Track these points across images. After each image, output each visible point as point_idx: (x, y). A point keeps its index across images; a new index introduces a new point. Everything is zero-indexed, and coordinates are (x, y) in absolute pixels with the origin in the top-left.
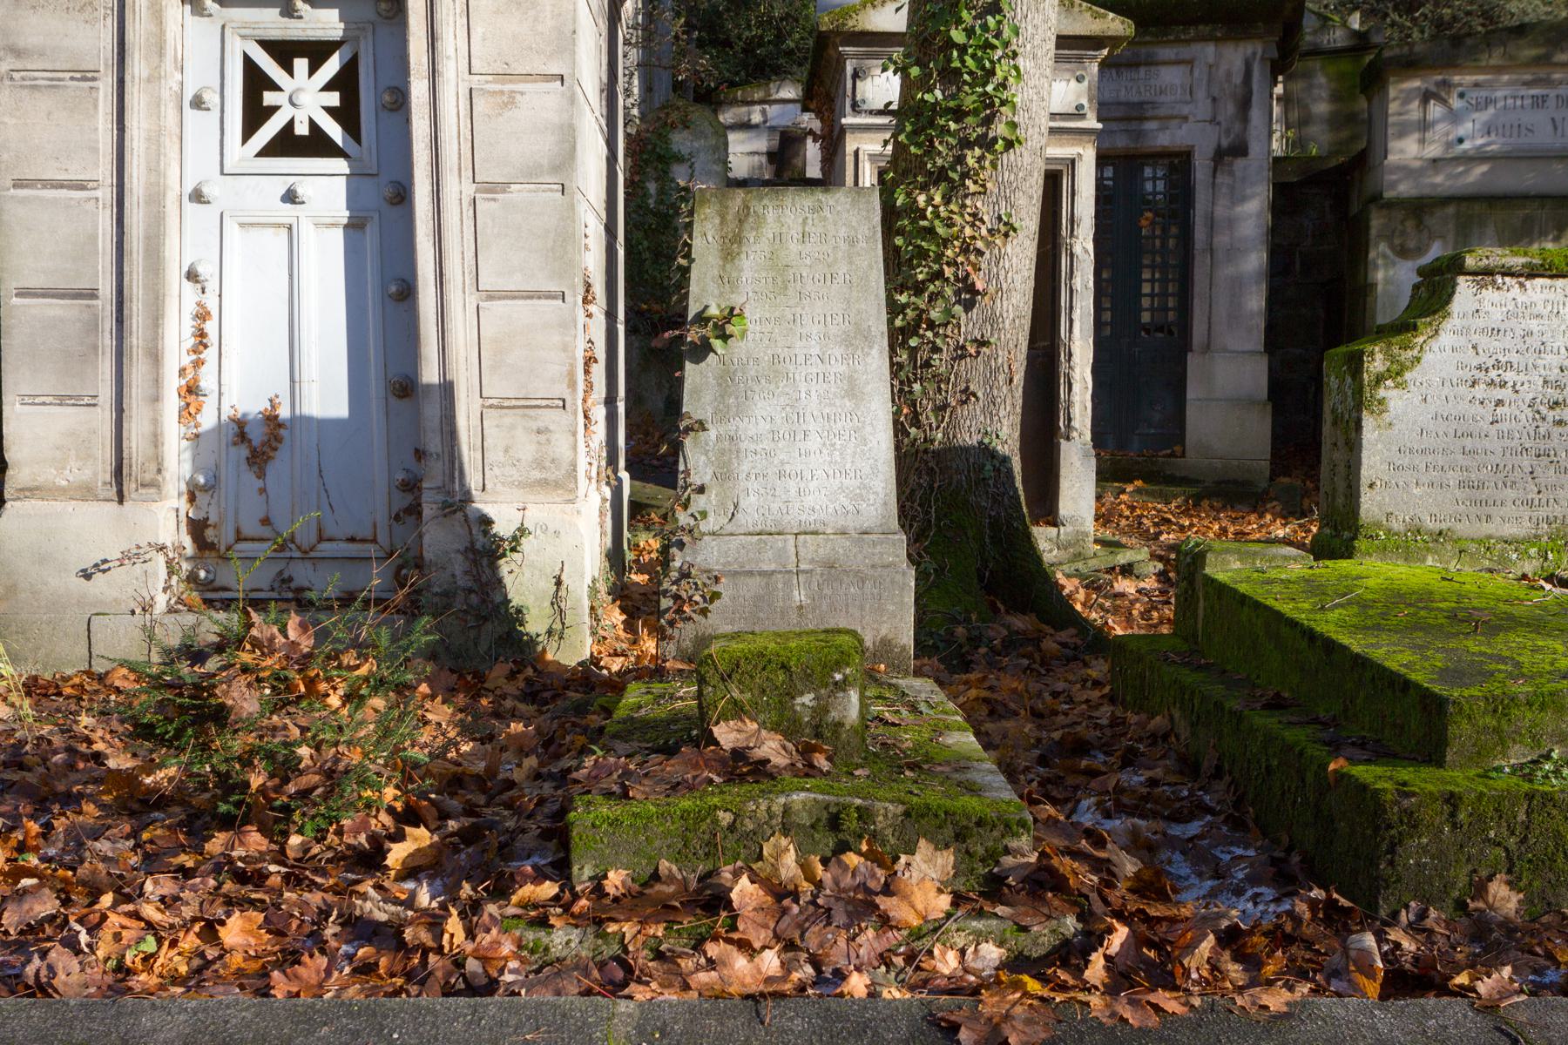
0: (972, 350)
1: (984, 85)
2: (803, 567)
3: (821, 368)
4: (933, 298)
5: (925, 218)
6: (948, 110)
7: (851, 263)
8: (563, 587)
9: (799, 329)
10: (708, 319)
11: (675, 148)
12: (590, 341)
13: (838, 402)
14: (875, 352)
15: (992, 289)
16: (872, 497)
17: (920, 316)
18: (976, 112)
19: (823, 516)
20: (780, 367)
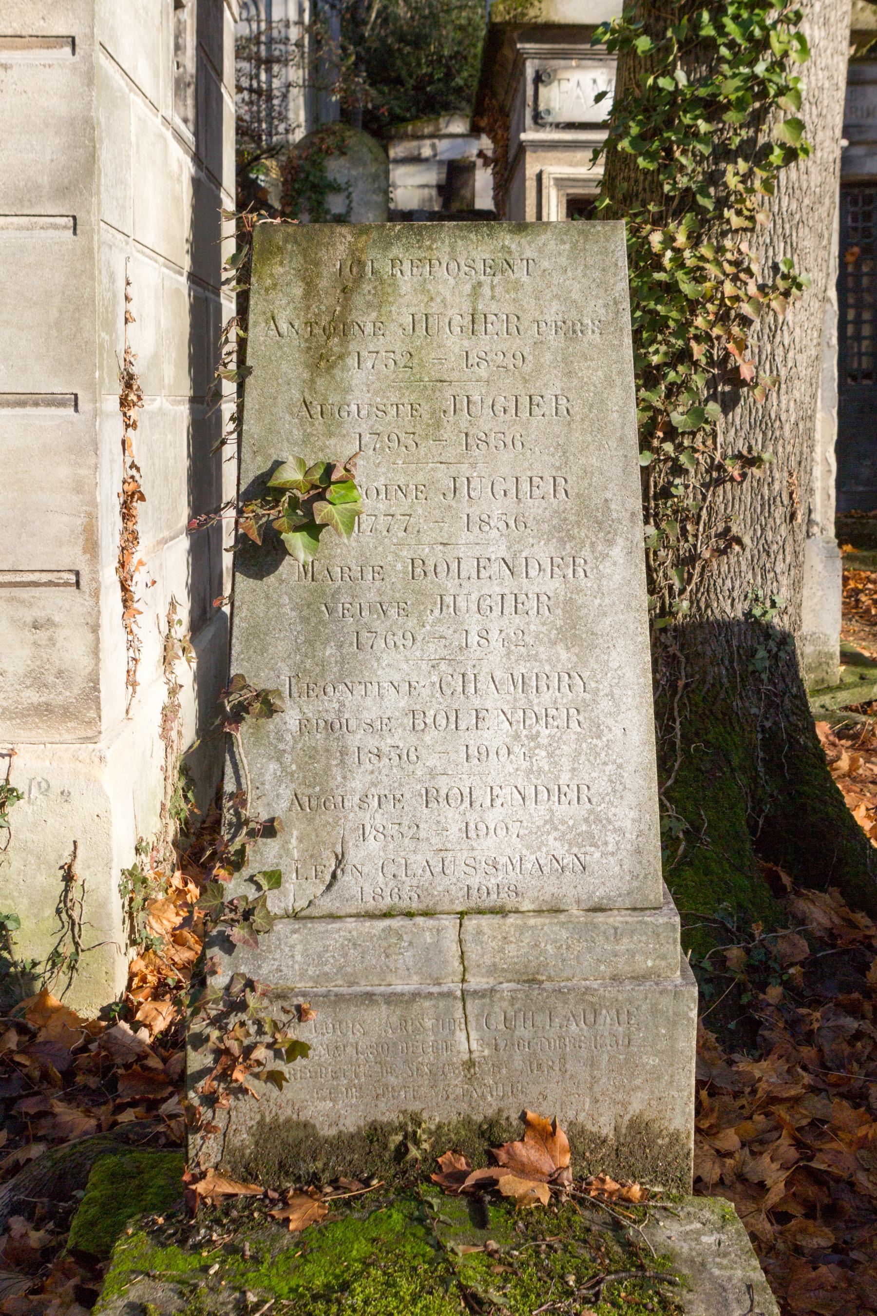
0: (733, 469)
1: (752, 64)
2: (475, 982)
3: (509, 585)
4: (672, 391)
5: (660, 268)
6: (696, 102)
7: (569, 374)
8: (76, 885)
9: (464, 507)
10: (281, 491)
11: (330, 176)
12: (133, 466)
14: (617, 552)
15: (765, 378)
16: (611, 838)
17: (653, 419)
18: (740, 105)
19: (513, 877)
20: (425, 584)
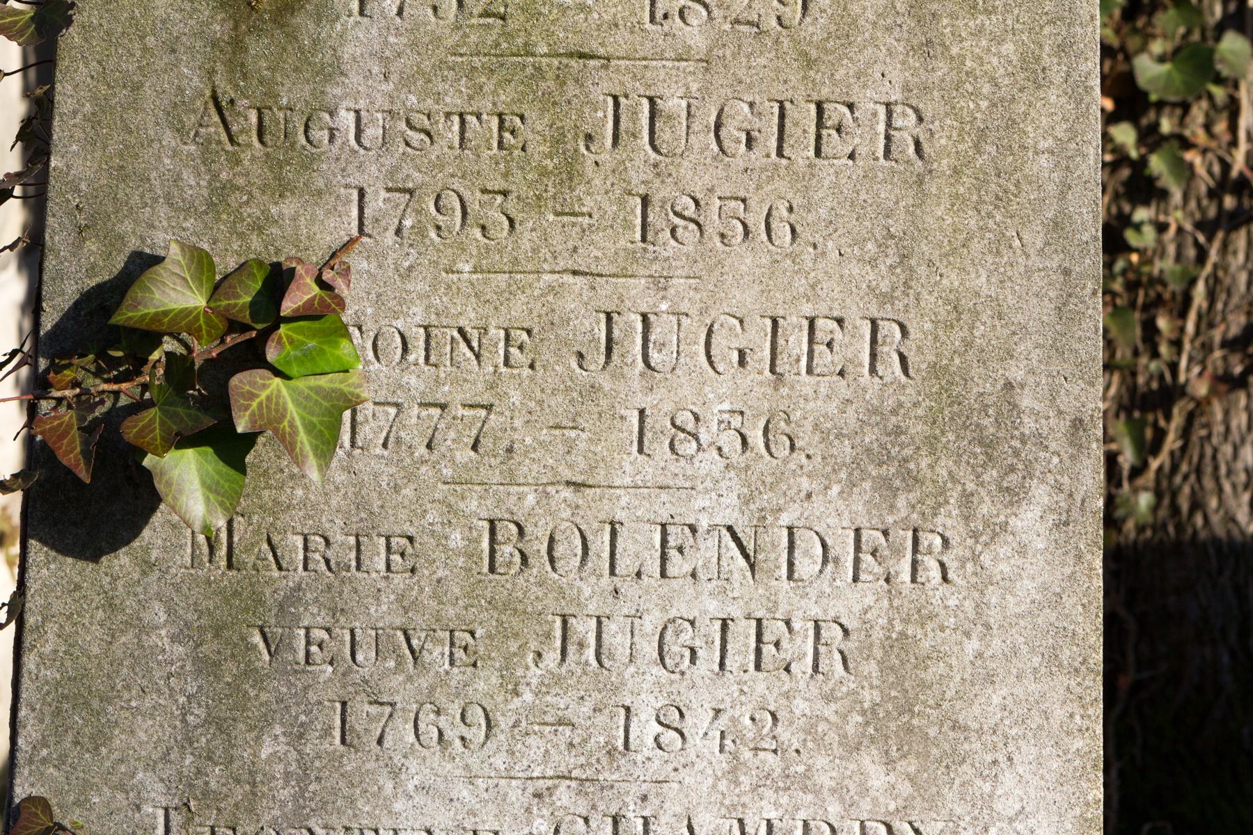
3: (744, 595)
7: (927, 48)
9: (630, 391)
13: (825, 770)
14: (1030, 521)
